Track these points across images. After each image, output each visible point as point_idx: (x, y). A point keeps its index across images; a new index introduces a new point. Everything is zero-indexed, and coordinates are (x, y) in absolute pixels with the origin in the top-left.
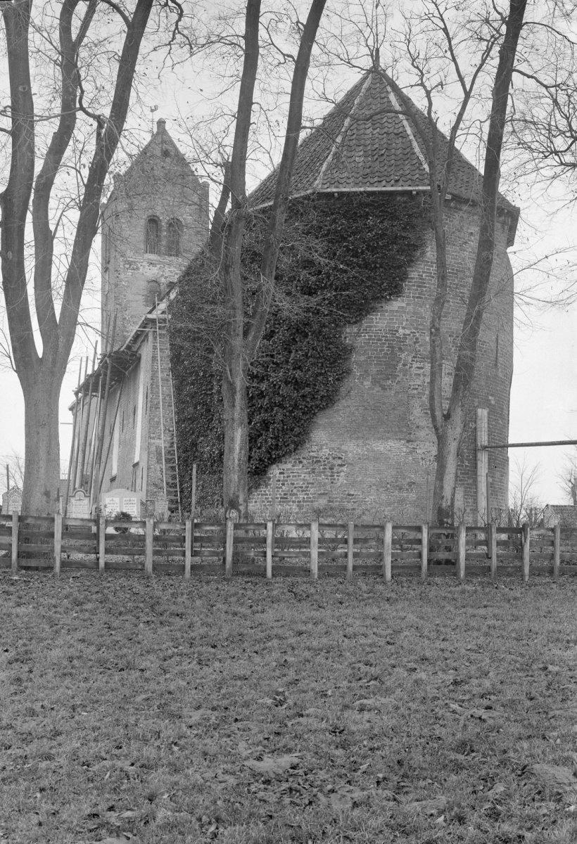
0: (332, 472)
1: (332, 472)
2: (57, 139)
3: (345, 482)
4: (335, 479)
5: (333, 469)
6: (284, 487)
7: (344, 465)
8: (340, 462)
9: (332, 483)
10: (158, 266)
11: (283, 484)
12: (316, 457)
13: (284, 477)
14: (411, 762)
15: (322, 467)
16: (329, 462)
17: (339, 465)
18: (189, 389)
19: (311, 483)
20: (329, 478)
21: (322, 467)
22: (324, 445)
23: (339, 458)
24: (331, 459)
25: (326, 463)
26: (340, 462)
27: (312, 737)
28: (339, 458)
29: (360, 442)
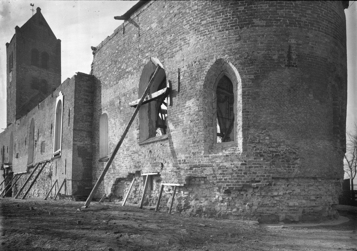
0: (289, 164)
1: (289, 164)
2: (8, 59)
3: (299, 172)
4: (291, 170)
5: (289, 161)
6: (246, 176)
7: (298, 159)
8: (294, 156)
9: (289, 172)
10: (38, 72)
11: (245, 173)
12: (276, 152)
13: (246, 168)
14: (96, 121)
15: (280, 160)
16: (286, 157)
17: (293, 158)
18: (6, 177)
19: (272, 173)
20: (287, 169)
21: (280, 160)
22: (281, 142)
23: (294, 153)
24: (288, 154)
25: (284, 156)
26: (294, 156)
27: (142, 158)
28: (294, 153)
29: (308, 140)
